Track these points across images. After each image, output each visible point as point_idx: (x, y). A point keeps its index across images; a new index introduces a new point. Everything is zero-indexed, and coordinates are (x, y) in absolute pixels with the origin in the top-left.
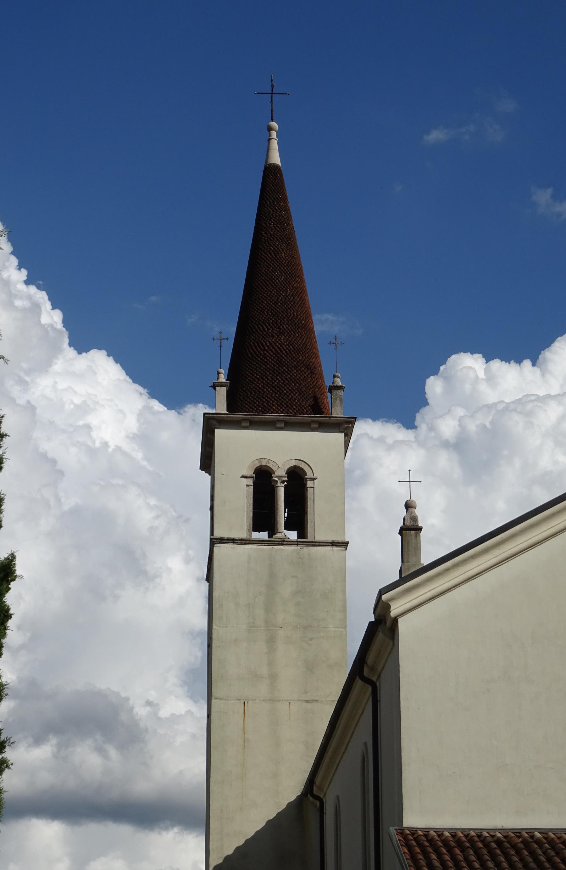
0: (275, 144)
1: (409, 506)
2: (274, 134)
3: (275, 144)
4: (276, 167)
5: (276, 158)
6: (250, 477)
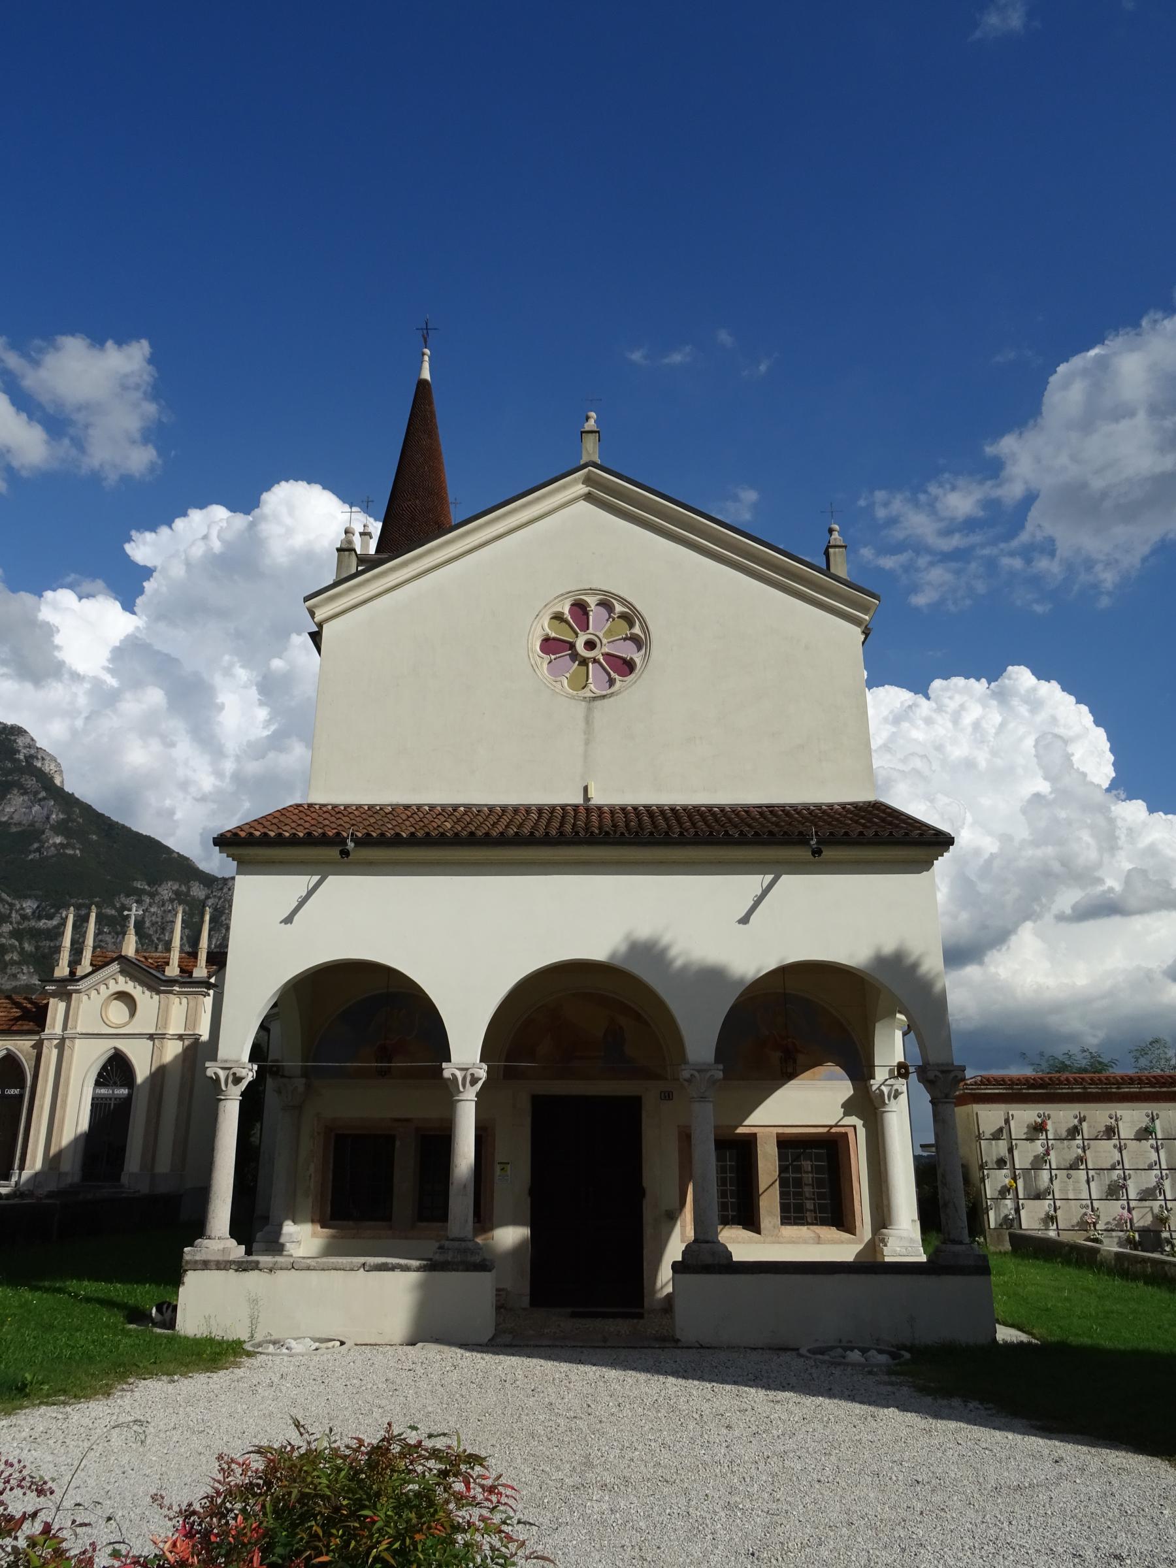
0: (426, 365)
2: (426, 358)
3: (426, 365)
4: (426, 381)
5: (426, 374)
6: (587, 798)
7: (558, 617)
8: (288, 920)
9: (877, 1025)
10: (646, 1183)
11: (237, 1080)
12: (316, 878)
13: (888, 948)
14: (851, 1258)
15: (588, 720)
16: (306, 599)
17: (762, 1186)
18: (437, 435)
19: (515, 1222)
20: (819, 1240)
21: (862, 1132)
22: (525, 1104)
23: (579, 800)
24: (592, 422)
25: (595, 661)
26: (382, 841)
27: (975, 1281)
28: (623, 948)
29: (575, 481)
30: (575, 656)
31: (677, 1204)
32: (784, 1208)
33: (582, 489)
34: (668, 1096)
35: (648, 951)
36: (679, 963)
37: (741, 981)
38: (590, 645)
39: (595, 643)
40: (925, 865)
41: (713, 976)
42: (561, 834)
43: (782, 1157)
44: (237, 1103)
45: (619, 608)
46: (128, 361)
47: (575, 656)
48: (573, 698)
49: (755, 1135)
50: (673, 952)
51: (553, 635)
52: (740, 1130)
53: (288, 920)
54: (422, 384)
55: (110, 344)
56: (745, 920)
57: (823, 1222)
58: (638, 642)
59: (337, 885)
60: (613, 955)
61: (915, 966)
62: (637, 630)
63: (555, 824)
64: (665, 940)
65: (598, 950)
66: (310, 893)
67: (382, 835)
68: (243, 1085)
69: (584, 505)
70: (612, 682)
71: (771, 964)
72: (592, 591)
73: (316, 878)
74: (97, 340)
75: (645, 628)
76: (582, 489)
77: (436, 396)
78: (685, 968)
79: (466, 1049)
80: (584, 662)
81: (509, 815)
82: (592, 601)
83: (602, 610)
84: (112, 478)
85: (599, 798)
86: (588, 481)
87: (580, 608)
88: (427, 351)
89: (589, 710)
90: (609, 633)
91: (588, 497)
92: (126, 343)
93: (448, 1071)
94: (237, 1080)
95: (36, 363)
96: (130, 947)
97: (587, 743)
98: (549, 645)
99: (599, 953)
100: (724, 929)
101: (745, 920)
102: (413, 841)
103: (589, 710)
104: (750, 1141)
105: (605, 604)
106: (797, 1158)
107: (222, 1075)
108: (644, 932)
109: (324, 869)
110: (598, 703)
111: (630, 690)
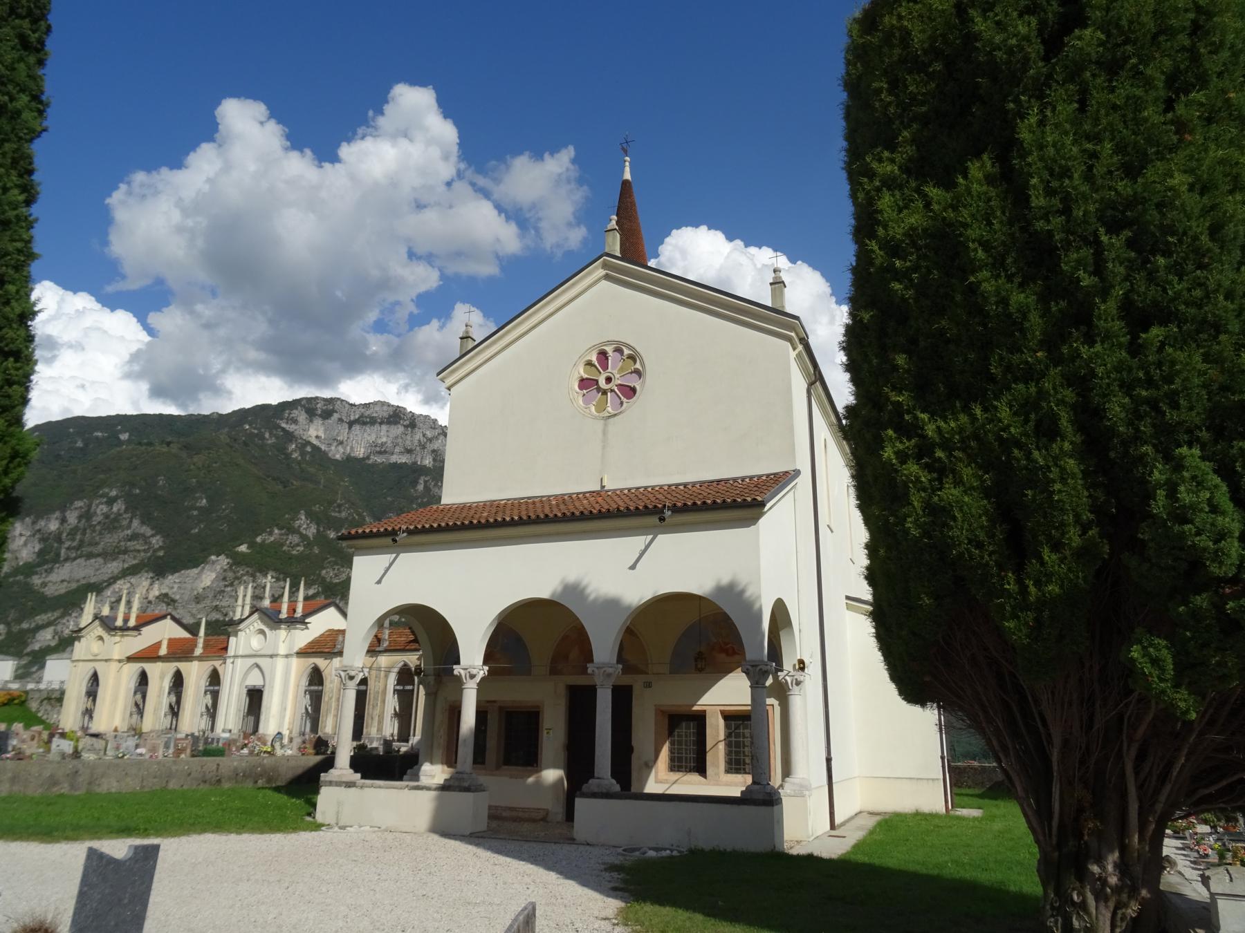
0: (627, 169)
3: (627, 169)
5: (627, 176)
6: (603, 487)
7: (589, 363)
8: (379, 582)
9: (781, 633)
10: (634, 743)
11: (472, 677)
12: (650, 537)
13: (725, 580)
14: (738, 795)
15: (605, 433)
16: (438, 374)
17: (722, 746)
18: (636, 218)
19: (555, 767)
20: (689, 783)
21: (777, 709)
22: (562, 690)
23: (598, 488)
24: (614, 222)
25: (612, 391)
26: (685, 509)
27: (762, 809)
28: (560, 589)
29: (596, 268)
30: (599, 389)
31: (653, 758)
32: (672, 759)
33: (602, 272)
34: (648, 685)
35: (574, 590)
36: (592, 597)
37: (629, 607)
38: (609, 380)
39: (612, 377)
40: (754, 520)
41: (612, 604)
42: (520, 518)
43: (727, 726)
44: (475, 692)
45: (626, 352)
46: (560, 163)
47: (599, 389)
48: (595, 418)
49: (705, 711)
50: (588, 591)
51: (586, 376)
52: (695, 708)
53: (379, 582)
54: (626, 183)
55: (546, 156)
56: (633, 567)
57: (690, 770)
58: (638, 372)
59: (664, 540)
60: (553, 595)
61: (743, 592)
62: (638, 366)
63: (516, 512)
64: (584, 583)
65: (544, 592)
66: (647, 547)
67: (714, 502)
68: (478, 679)
69: (604, 283)
70: (622, 403)
71: (648, 596)
72: (609, 343)
73: (650, 537)
74: (538, 156)
75: (643, 364)
76: (602, 272)
77: (635, 189)
78: (595, 600)
79: (472, 656)
80: (605, 393)
81: (487, 508)
82: (609, 349)
83: (617, 354)
84: (559, 254)
85: (609, 485)
86: (605, 266)
87: (603, 355)
88: (628, 158)
89: (606, 425)
90: (621, 369)
91: (607, 277)
92: (558, 152)
93: (457, 670)
94: (472, 677)
95: (497, 181)
96: (267, 603)
97: (604, 447)
98: (584, 383)
99: (545, 594)
100: (620, 574)
101: (633, 567)
102: (521, 522)
103: (606, 425)
104: (700, 719)
105: (618, 350)
106: (737, 727)
107: (463, 672)
108: (572, 578)
109: (655, 531)
110: (611, 420)
111: (633, 407)
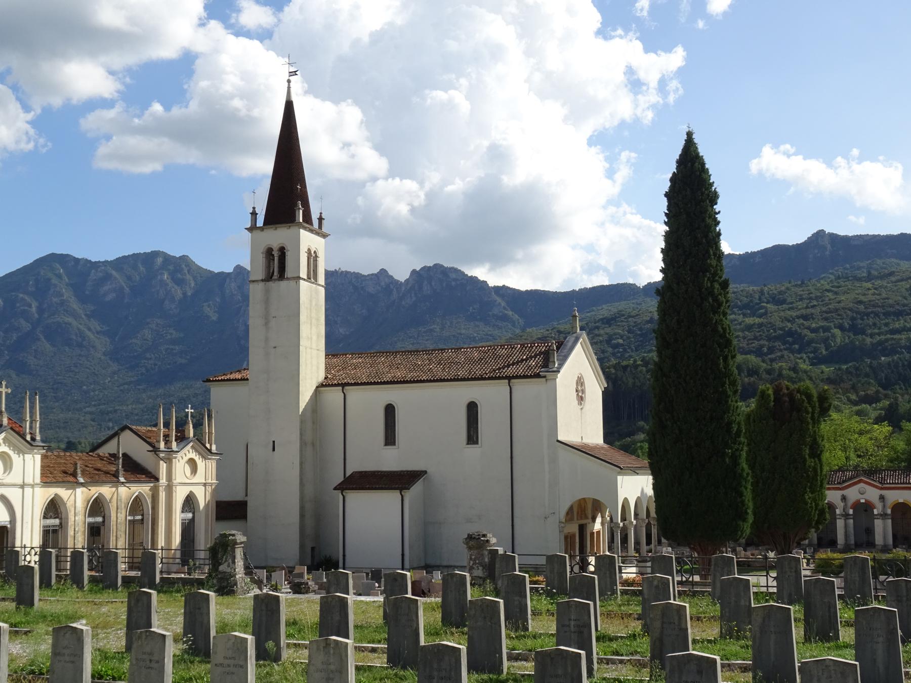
1: (254, 208)
85: (586, 441)
